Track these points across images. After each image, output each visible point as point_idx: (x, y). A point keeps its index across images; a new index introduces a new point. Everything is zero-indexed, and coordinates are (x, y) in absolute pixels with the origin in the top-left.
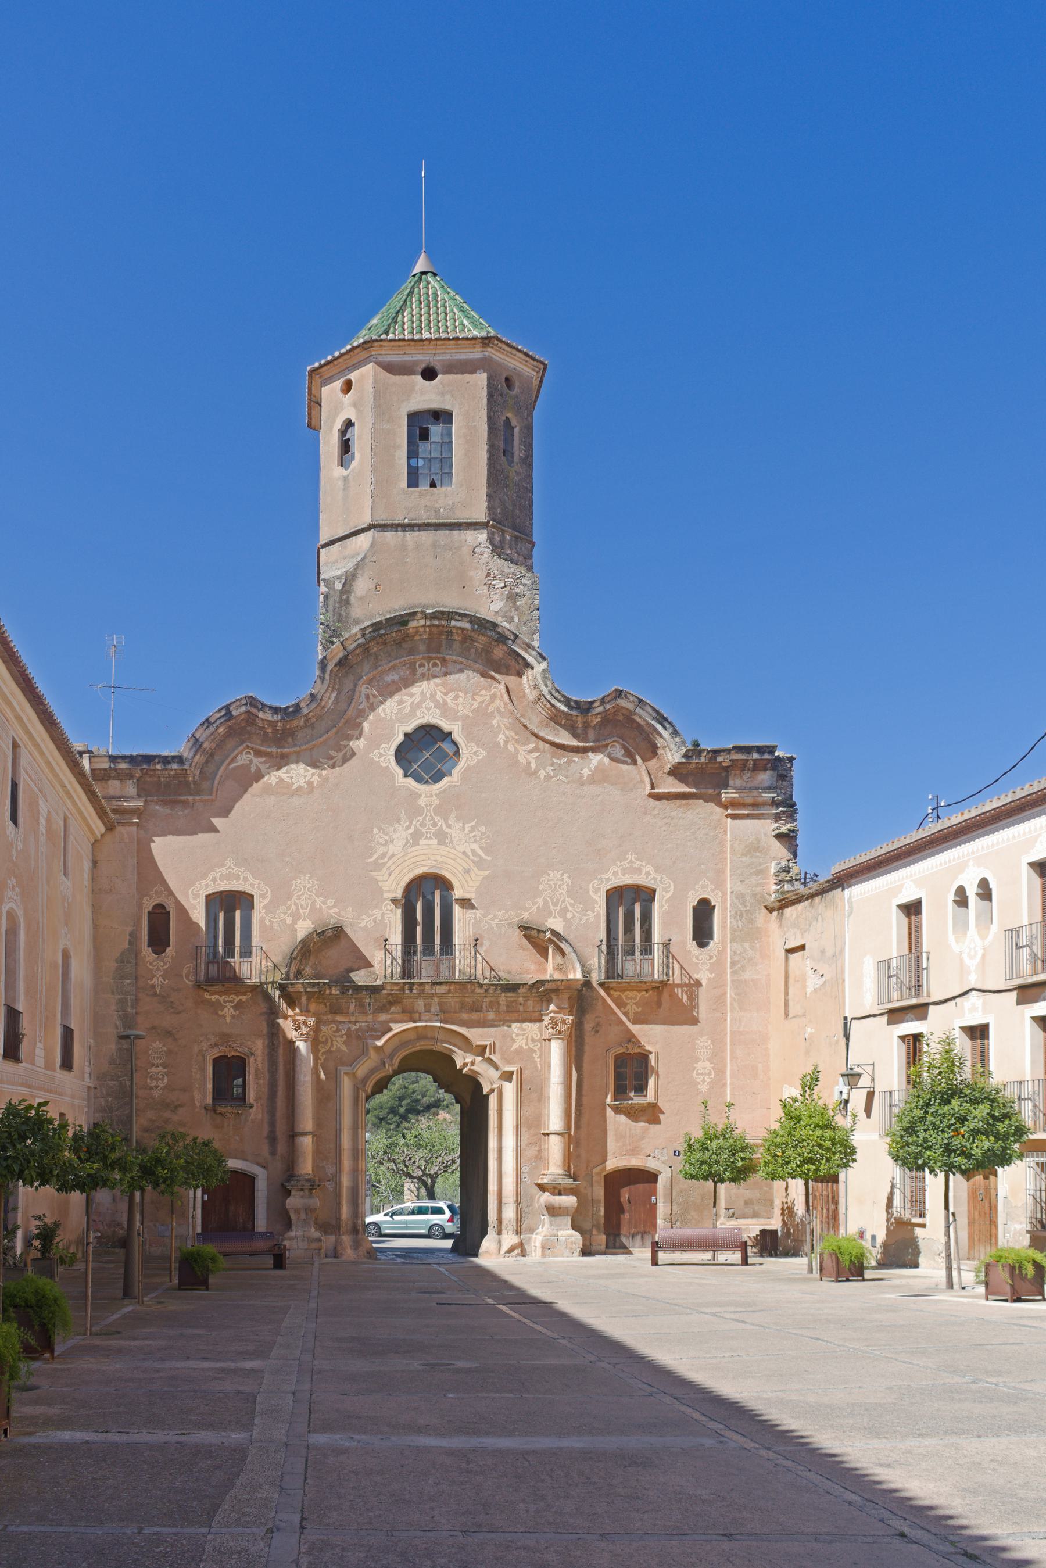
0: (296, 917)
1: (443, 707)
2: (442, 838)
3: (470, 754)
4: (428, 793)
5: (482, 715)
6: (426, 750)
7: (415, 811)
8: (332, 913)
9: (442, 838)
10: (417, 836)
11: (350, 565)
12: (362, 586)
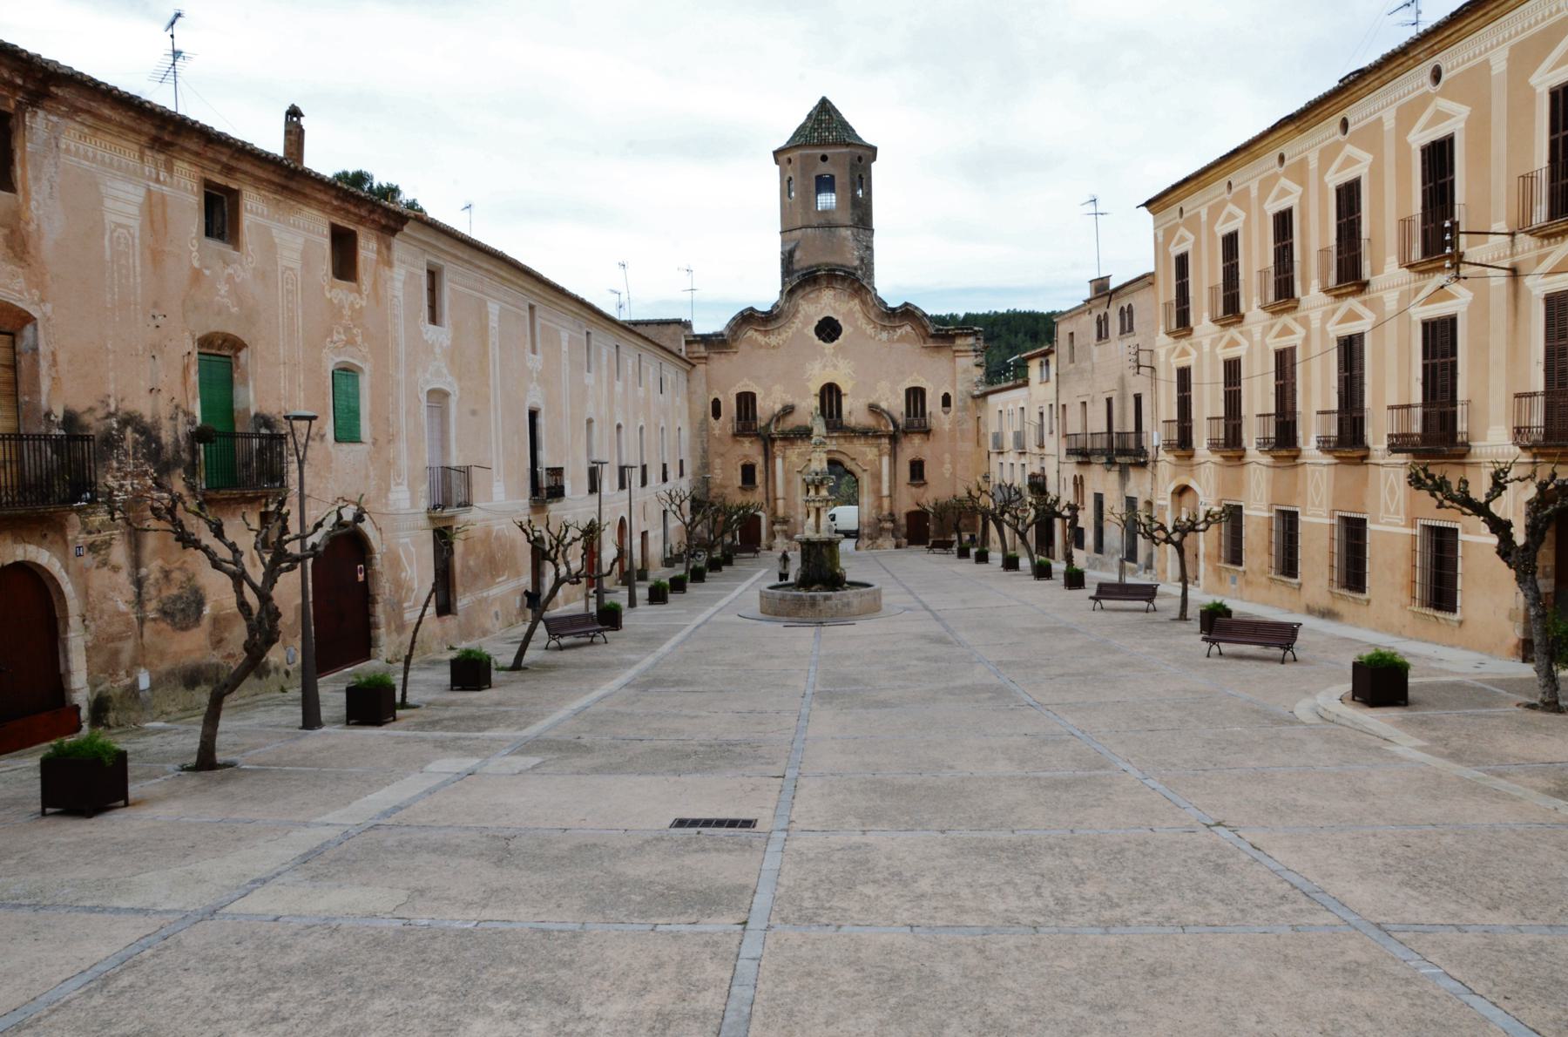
1: (834, 309)
2: (835, 367)
4: (829, 347)
5: (851, 311)
6: (828, 330)
8: (789, 400)
9: (835, 367)
10: (825, 367)
11: (793, 244)
12: (798, 255)
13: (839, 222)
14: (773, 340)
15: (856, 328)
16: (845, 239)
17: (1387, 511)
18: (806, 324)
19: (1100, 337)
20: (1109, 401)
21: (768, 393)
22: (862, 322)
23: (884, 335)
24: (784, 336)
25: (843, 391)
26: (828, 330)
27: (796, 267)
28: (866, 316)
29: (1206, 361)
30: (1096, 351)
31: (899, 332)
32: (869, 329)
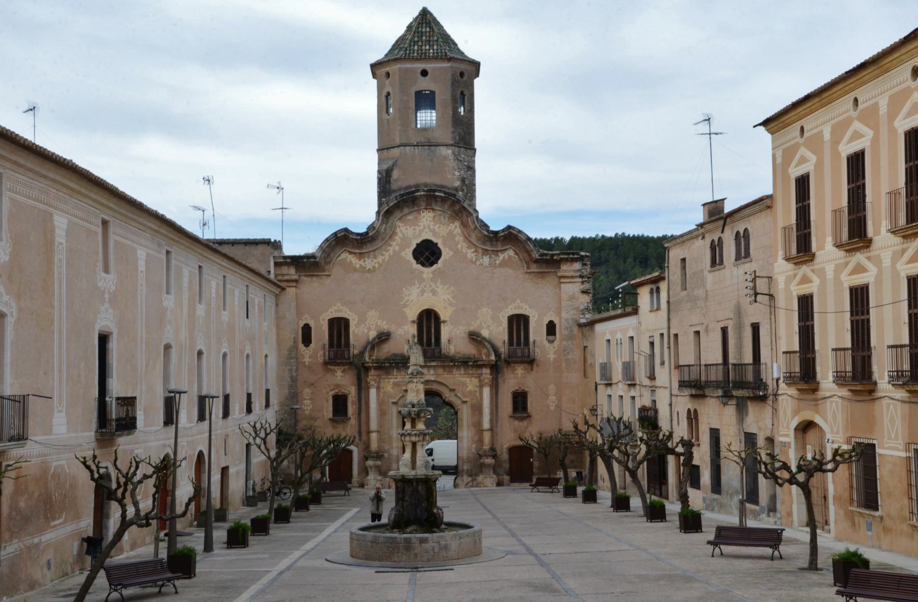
0: (369, 329)
1: (433, 231)
2: (434, 292)
3: (446, 253)
4: (427, 272)
5: (451, 235)
6: (427, 253)
7: (422, 280)
8: (385, 326)
9: (434, 292)
10: (423, 292)
11: (391, 163)
12: (395, 174)
13: (441, 141)
14: (369, 263)
15: (457, 252)
16: (445, 158)
17: (890, 438)
18: (403, 247)
19: (713, 263)
20: (724, 331)
21: (362, 320)
22: (462, 245)
23: (486, 260)
24: (380, 259)
25: (442, 318)
26: (427, 253)
27: (394, 186)
28: (467, 239)
29: (830, 288)
30: (710, 278)
31: (501, 256)
32: (470, 254)
